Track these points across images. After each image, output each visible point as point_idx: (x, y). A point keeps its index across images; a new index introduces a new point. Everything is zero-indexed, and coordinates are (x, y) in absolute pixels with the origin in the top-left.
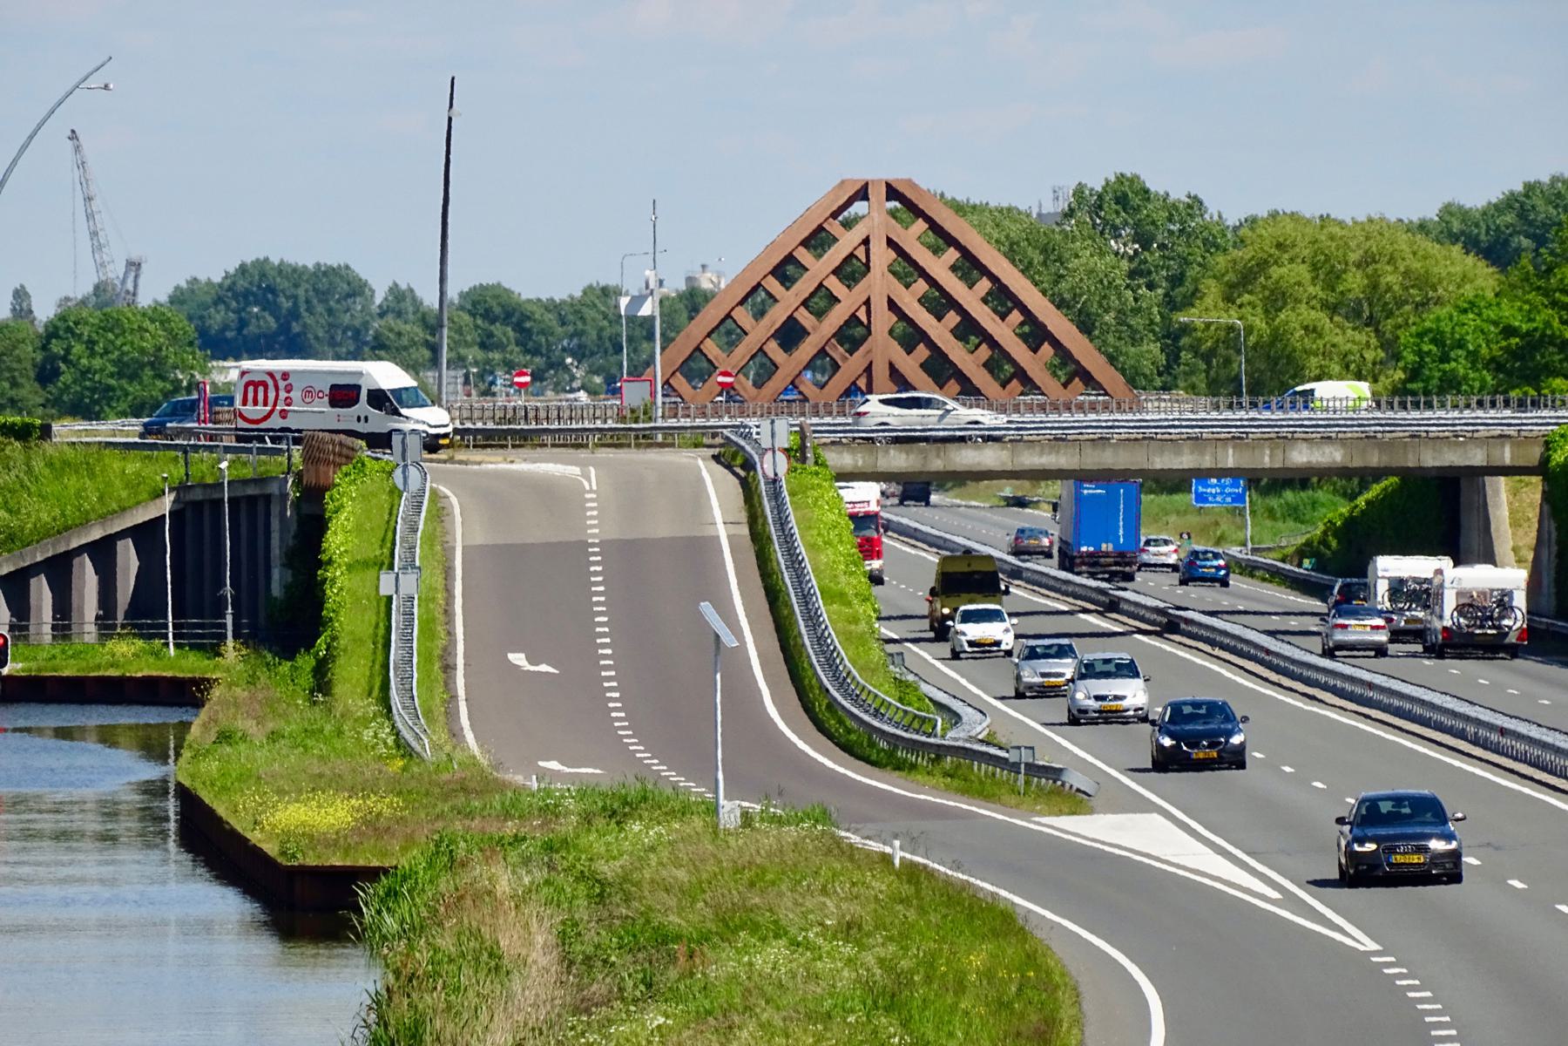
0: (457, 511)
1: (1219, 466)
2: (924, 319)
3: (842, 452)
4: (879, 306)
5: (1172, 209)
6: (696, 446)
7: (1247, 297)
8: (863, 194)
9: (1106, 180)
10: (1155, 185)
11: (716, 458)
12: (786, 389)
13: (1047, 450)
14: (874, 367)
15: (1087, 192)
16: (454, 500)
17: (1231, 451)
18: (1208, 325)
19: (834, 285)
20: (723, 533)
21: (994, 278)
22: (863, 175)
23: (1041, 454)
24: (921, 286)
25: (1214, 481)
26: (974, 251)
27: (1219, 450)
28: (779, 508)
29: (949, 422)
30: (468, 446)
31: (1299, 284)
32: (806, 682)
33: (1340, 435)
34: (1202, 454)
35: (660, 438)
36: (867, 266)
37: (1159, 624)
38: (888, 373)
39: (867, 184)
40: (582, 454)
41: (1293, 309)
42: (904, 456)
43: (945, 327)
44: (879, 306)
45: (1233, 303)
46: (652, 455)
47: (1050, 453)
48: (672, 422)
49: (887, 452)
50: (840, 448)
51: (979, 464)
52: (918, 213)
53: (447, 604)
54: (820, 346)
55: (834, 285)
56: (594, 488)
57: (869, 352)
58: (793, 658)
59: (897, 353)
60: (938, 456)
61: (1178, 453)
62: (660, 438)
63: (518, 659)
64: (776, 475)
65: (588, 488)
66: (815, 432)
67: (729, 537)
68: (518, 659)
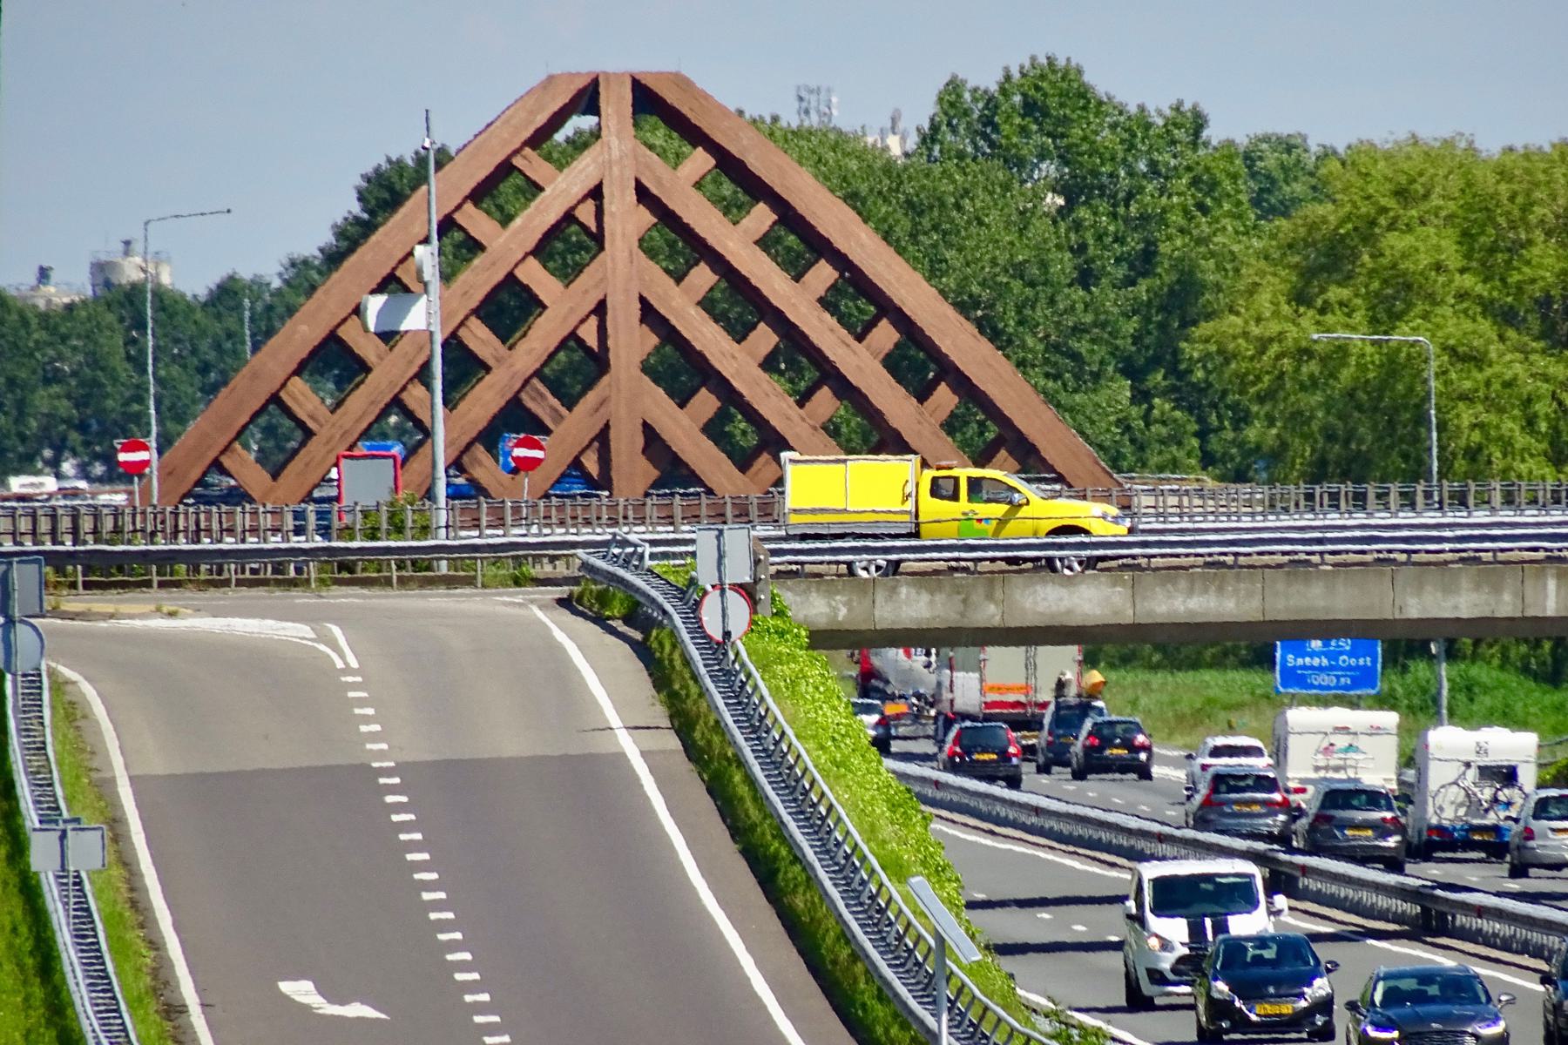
0: (99, 710)
1: (1530, 613)
2: (708, 337)
3: (807, 591)
4: (624, 318)
5: (1136, 128)
6: (517, 582)
7: (1335, 293)
8: (588, 99)
9: (1007, 71)
10: (1100, 80)
11: (564, 603)
12: (563, 475)
13: (1198, 585)
14: (612, 434)
15: (967, 96)
16: (88, 689)
17: (1552, 584)
18: (1263, 344)
19: (535, 275)
20: (628, 744)
21: (840, 261)
22: (580, 63)
23: (1190, 592)
24: (703, 277)
25: (1316, 644)
26: (801, 209)
27: (1529, 583)
28: (739, 695)
29: (1015, 531)
30: (73, 585)
31: (1439, 267)
32: (879, 1030)
33: (1242, 560)
34: (1497, 589)
35: (443, 568)
36: (598, 239)
37: (1398, 918)
38: (640, 441)
39: (595, 83)
40: (299, 597)
41: (1425, 316)
42: (925, 597)
43: (750, 354)
44: (624, 318)
45: (1309, 305)
46: (438, 601)
47: (1206, 591)
48: (470, 537)
49: (893, 590)
50: (801, 584)
51: (1069, 612)
52: (695, 136)
53: (132, 890)
54: (509, 395)
55: (535, 275)
56: (354, 664)
57: (603, 402)
58: (837, 983)
59: (658, 405)
60: (990, 597)
61: (1449, 589)
62: (443, 568)
63: (301, 991)
64: (727, 634)
65: (340, 664)
66: (774, 553)
67: (644, 754)
68: (301, 991)
